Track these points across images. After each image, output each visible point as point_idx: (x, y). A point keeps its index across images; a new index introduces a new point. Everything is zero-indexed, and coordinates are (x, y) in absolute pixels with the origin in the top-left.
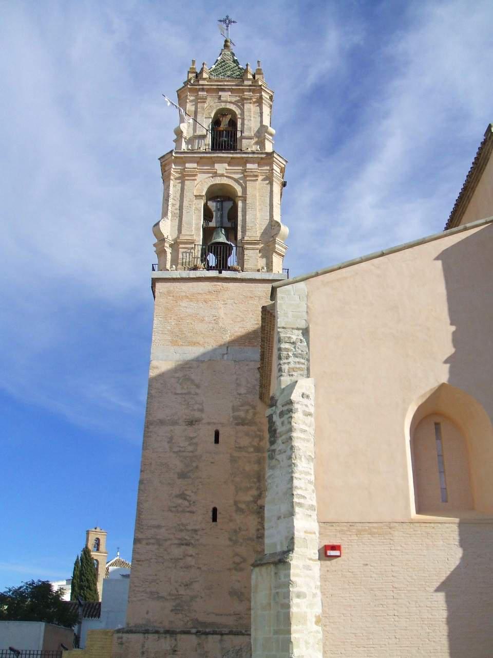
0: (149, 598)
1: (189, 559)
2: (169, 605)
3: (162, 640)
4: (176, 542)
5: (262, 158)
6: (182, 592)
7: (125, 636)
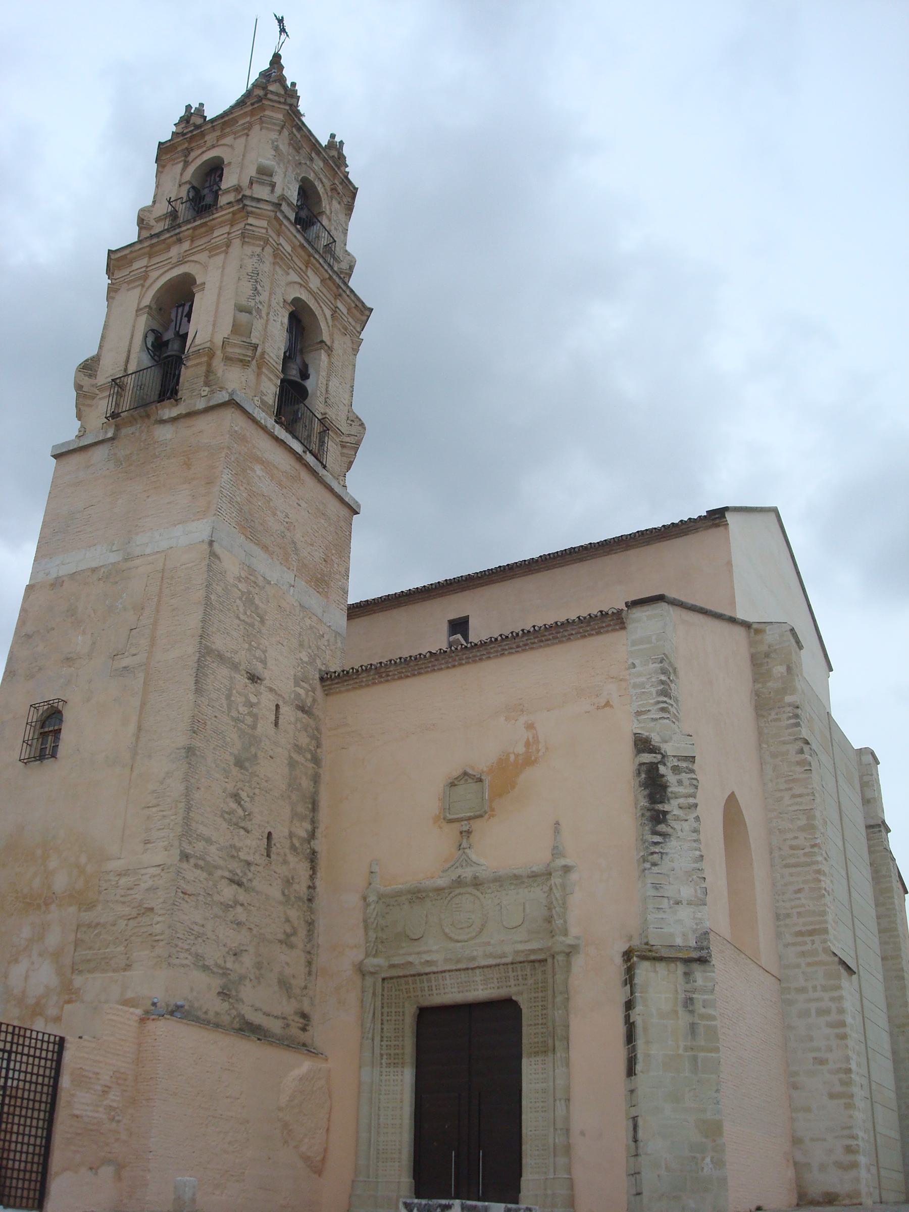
1: (239, 909)
2: (217, 983)
4: (227, 874)
6: (229, 965)
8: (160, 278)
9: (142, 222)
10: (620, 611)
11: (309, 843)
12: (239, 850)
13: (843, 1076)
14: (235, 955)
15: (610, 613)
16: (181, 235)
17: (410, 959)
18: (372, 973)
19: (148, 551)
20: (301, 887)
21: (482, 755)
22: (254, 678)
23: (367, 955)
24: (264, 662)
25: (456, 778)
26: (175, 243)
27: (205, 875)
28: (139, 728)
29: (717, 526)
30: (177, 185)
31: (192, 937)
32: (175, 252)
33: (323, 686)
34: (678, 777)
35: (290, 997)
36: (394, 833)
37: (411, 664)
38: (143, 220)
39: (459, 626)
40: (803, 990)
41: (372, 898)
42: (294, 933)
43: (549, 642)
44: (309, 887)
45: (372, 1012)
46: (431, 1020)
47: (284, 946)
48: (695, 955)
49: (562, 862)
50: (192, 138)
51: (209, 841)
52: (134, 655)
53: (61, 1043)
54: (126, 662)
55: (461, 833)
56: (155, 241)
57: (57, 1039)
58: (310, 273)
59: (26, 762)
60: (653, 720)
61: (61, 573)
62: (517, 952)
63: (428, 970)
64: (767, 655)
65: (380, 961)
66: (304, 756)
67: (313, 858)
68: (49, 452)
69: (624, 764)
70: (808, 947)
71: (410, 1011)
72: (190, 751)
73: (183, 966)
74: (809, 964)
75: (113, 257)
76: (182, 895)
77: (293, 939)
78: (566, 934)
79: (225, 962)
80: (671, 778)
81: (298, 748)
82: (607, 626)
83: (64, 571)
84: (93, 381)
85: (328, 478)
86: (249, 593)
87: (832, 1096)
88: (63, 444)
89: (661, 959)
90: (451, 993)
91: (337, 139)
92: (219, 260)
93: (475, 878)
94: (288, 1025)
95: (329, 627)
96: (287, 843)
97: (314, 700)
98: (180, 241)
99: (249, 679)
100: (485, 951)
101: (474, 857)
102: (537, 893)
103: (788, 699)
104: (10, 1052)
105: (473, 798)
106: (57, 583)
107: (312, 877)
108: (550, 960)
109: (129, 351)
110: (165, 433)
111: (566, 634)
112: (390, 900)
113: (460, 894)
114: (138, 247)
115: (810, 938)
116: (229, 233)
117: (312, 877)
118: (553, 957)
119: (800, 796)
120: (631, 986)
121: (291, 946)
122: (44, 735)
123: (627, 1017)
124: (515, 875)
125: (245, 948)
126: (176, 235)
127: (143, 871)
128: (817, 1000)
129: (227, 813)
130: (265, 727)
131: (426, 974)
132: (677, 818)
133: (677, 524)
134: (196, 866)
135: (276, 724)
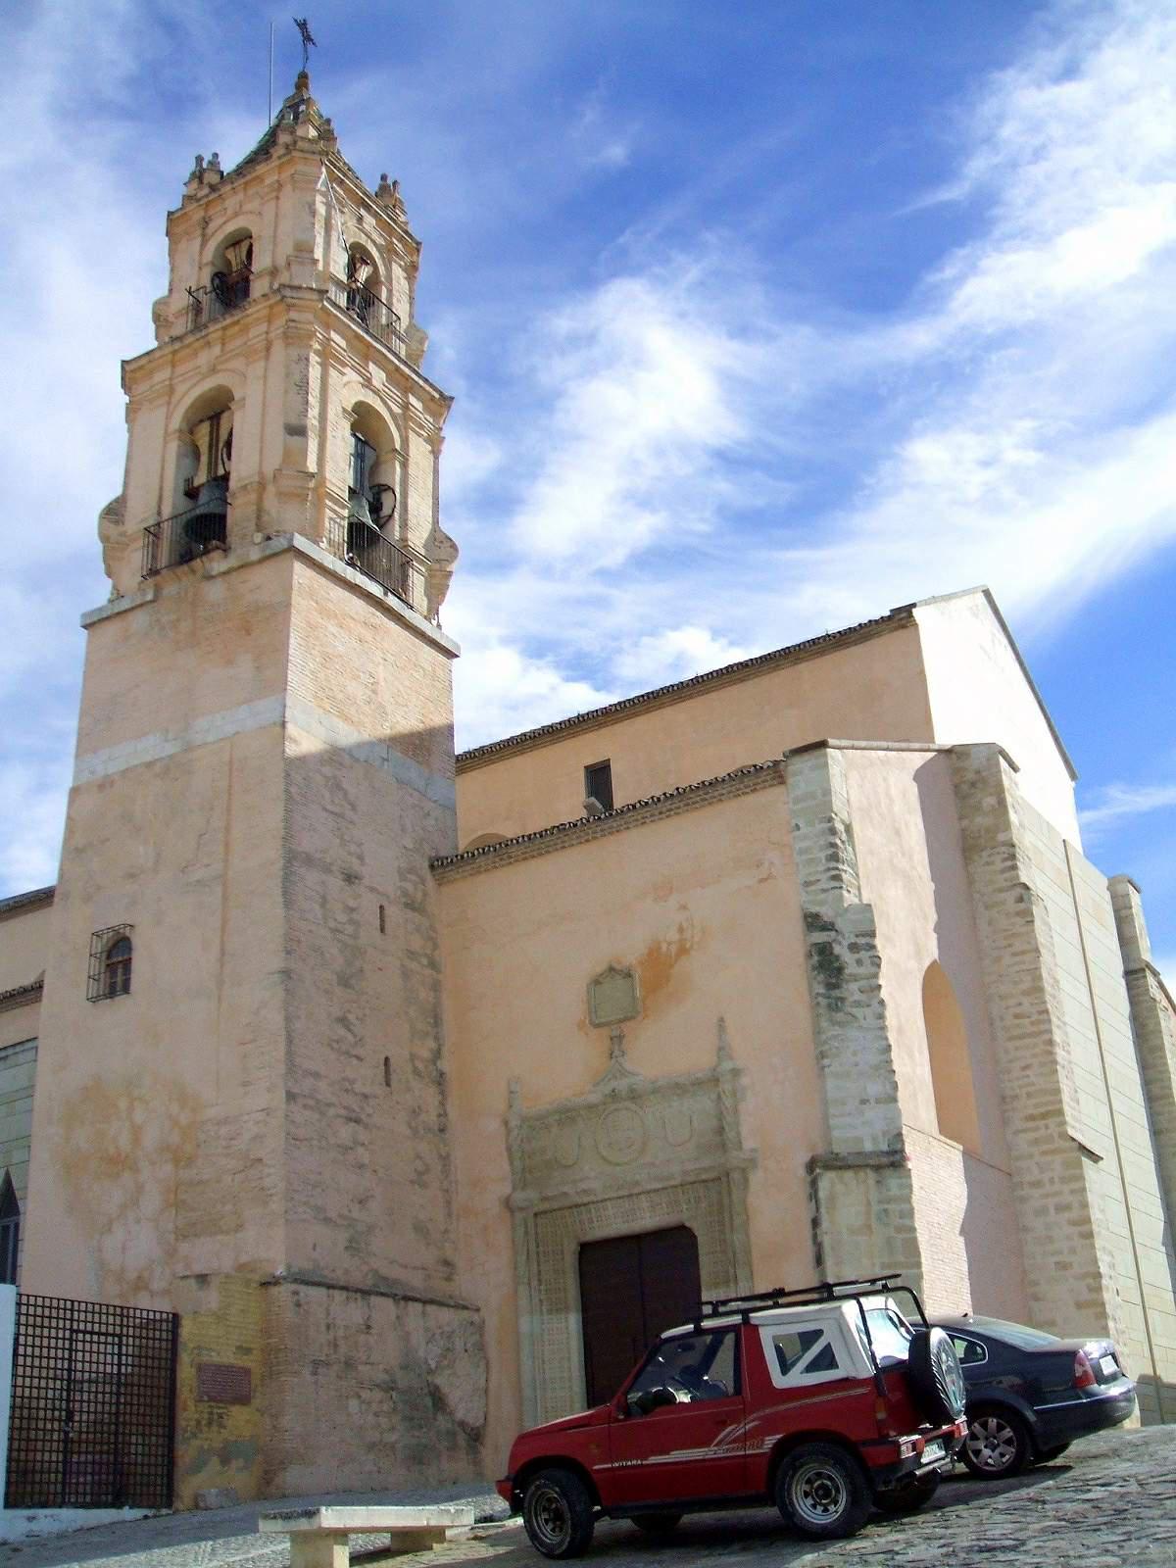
0: (315, 1218)
1: (361, 1150)
2: (343, 1237)
3: (352, 1305)
4: (343, 1112)
5: (433, 398)
6: (355, 1214)
7: (303, 1288)
8: (190, 393)
9: (159, 318)
10: (776, 763)
11: (435, 1064)
12: (352, 1082)
13: (1090, 1281)
14: (360, 1202)
15: (765, 767)
16: (209, 337)
17: (565, 1189)
18: (521, 1209)
19: (210, 738)
20: (431, 1117)
21: (631, 949)
22: (350, 878)
23: (514, 1189)
24: (361, 858)
25: (601, 975)
26: (202, 347)
27: (317, 1116)
28: (223, 952)
29: (904, 627)
30: (197, 269)
31: (310, 1188)
32: (204, 358)
33: (434, 876)
34: (857, 956)
35: (428, 1244)
36: (531, 1045)
37: (537, 842)
38: (160, 315)
39: (599, 778)
40: (1037, 1184)
41: (514, 1123)
42: (428, 1170)
43: (697, 805)
44: (440, 1115)
45: (525, 1253)
46: (595, 1257)
47: (417, 1187)
48: (885, 1160)
49: (727, 1065)
50: (208, 204)
51: (317, 1075)
52: (208, 865)
53: (175, 1320)
54: (199, 874)
55: (611, 1039)
56: (177, 345)
57: (171, 1316)
58: (372, 367)
59: (94, 1000)
60: (824, 891)
61: (110, 772)
62: (685, 1173)
63: (586, 1200)
64: (973, 784)
65: (532, 1194)
66: (419, 963)
67: (440, 1080)
68: (78, 621)
69: (795, 942)
70: (1042, 1132)
71: (570, 1250)
72: (286, 973)
73: (304, 1221)
74: (1045, 1153)
75: (127, 368)
76: (293, 1142)
77: (425, 1177)
78: (741, 1148)
79: (350, 1211)
80: (848, 957)
81: (412, 954)
82: (763, 782)
83: (113, 768)
84: (121, 529)
85: (415, 618)
86: (335, 777)
87: (1079, 1306)
88: (93, 612)
89: (849, 1167)
90: (613, 1223)
91: (390, 182)
92: (259, 367)
93: (632, 1090)
94: (429, 1276)
95: (435, 802)
96: (409, 1068)
97: (425, 894)
98: (208, 344)
99: (345, 880)
100: (649, 1173)
101: (628, 1066)
102: (705, 1102)
103: (1001, 837)
104: (120, 1336)
105: (624, 996)
106: (105, 784)
107: (442, 1104)
108: (724, 1179)
109: (161, 489)
110: (215, 591)
111: (716, 794)
112: (537, 1123)
113: (616, 1110)
114: (158, 354)
115: (1043, 1122)
116: (267, 333)
117: (442, 1104)
118: (728, 1175)
119: (1023, 953)
120: (816, 1202)
121: (424, 1185)
122: (111, 968)
123: (815, 1236)
124: (677, 1084)
125: (284, 159)
126: (203, 337)
127: (246, 1118)
128: (1056, 1194)
129: (334, 1041)
130: (369, 934)
131: (585, 1205)
132: (858, 1004)
133: (855, 628)
134: (305, 1106)
135: (382, 930)
